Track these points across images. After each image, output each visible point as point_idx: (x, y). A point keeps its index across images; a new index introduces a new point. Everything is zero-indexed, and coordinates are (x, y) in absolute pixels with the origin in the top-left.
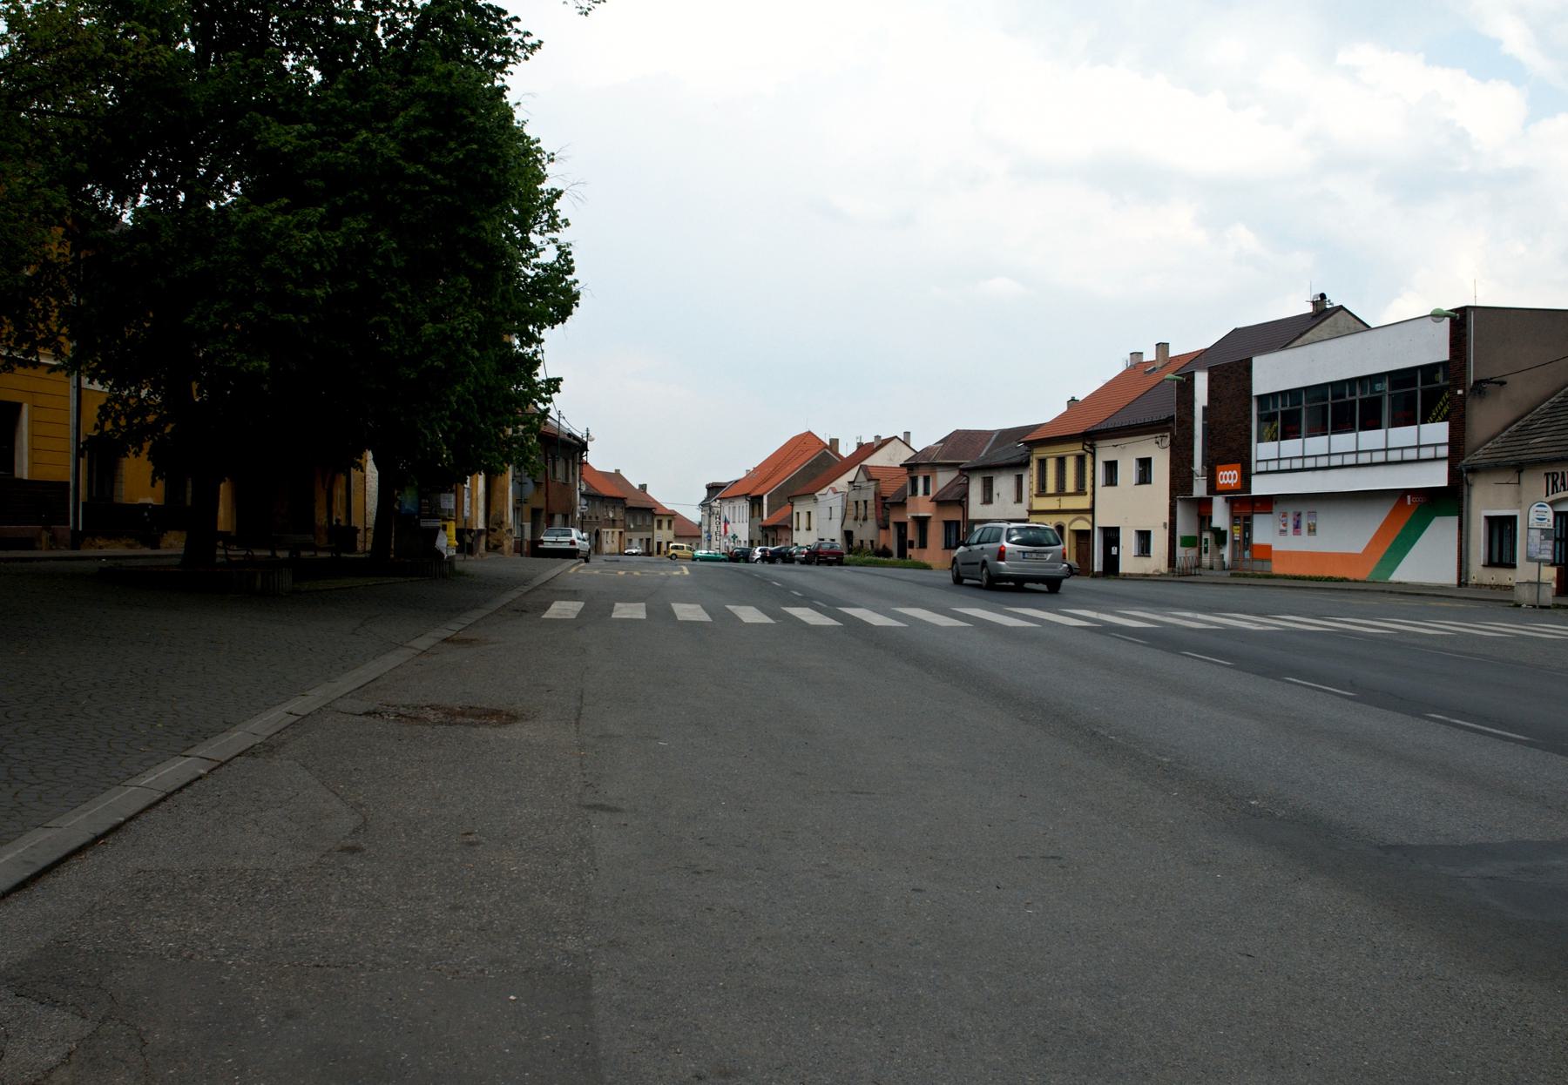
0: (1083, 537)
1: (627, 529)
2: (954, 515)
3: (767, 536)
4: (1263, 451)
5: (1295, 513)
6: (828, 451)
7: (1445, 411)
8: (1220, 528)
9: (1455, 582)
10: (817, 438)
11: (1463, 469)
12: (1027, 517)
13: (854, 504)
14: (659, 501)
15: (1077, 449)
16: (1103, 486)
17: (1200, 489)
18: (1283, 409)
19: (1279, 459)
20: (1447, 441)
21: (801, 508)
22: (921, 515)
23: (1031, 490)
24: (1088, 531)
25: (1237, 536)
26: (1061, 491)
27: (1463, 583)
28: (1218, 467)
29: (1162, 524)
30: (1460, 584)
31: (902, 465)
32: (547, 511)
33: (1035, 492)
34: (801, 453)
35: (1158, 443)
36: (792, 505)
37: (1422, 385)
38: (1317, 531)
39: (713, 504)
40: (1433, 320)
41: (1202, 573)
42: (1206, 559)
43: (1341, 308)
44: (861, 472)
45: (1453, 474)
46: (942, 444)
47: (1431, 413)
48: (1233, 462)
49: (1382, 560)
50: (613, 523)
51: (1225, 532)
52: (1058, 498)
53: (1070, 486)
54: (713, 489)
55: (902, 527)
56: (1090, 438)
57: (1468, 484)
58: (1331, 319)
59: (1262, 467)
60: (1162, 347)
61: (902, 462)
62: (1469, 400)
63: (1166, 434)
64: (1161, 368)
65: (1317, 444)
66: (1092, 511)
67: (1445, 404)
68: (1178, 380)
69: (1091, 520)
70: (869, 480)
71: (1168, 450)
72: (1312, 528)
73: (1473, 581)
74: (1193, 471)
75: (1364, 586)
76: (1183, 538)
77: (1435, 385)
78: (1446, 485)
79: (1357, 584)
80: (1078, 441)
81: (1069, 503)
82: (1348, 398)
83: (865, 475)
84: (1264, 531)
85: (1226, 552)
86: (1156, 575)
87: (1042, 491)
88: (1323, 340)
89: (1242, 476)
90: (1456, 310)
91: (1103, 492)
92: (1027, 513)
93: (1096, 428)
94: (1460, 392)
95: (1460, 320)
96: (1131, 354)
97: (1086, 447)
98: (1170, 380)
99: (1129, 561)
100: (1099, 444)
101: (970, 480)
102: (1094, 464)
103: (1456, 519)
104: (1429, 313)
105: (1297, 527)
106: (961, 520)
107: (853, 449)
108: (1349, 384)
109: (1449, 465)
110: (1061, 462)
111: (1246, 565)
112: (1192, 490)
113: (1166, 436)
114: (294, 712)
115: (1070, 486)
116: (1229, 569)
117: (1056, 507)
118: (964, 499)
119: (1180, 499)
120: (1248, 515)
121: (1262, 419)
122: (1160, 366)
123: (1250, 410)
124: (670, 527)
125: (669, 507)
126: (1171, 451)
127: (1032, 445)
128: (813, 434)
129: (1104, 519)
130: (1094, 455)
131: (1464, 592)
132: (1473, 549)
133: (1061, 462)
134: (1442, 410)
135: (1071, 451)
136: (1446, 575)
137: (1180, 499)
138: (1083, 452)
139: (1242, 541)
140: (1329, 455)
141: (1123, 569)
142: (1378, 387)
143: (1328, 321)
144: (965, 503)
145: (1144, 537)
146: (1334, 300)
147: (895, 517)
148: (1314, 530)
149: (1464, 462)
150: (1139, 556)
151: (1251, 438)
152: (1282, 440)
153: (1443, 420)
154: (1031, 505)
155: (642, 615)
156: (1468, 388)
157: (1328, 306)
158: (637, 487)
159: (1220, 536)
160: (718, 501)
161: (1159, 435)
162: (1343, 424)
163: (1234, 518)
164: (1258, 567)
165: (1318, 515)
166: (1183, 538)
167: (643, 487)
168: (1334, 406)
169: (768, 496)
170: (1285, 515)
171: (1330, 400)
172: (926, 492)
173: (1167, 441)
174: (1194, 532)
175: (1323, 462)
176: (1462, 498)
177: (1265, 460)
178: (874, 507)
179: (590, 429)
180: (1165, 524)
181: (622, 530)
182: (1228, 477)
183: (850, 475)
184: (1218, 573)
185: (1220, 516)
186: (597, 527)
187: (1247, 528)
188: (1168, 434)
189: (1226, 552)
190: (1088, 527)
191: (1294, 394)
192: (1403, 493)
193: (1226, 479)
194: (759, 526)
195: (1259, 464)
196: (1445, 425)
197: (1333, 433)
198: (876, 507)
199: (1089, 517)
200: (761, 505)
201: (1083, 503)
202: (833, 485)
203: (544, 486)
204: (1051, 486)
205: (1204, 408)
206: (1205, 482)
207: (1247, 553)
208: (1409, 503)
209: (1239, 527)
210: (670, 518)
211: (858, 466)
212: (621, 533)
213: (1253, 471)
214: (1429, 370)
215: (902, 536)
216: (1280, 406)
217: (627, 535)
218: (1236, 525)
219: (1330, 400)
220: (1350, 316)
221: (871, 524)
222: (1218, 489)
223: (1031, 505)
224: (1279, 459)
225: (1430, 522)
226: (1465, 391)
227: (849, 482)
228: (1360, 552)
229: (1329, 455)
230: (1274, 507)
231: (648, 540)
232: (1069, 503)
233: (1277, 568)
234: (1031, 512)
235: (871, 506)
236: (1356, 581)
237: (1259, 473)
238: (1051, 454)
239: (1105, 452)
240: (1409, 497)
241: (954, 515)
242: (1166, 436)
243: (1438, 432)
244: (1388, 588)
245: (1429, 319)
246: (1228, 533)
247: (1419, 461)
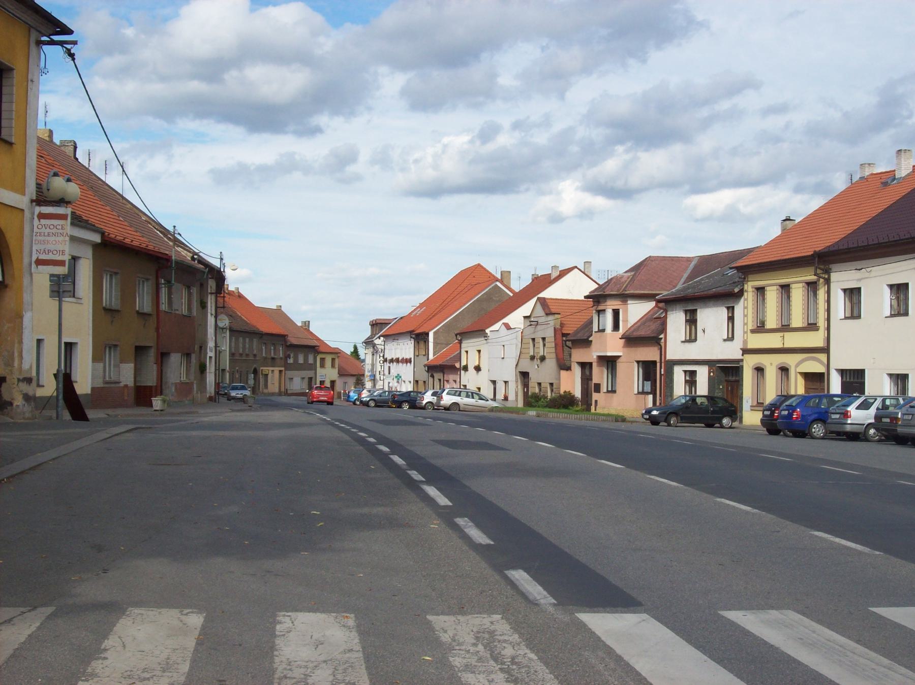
1: (288, 367)
2: (649, 354)
3: (433, 376)
6: (498, 284)
10: (488, 271)
12: (740, 357)
13: (531, 342)
14: (322, 338)
21: (470, 346)
22: (609, 354)
23: (745, 324)
24: (822, 375)
31: (585, 297)
32: (158, 349)
33: (750, 327)
34: (469, 287)
36: (460, 342)
39: (377, 342)
44: (539, 305)
46: (633, 273)
50: (273, 361)
52: (781, 334)
54: (377, 325)
55: (586, 366)
61: (587, 294)
66: (826, 350)
69: (826, 362)
70: (547, 314)
77: (726, 306)
83: (544, 309)
87: (760, 328)
91: (842, 329)
92: (741, 352)
93: (831, 249)
97: (819, 271)
100: (834, 267)
101: (668, 313)
106: (658, 360)
107: (527, 281)
118: (662, 336)
124: (333, 366)
125: (332, 345)
127: (748, 271)
128: (482, 267)
130: (828, 282)
135: (798, 281)
138: (815, 277)
144: (663, 341)
147: (579, 355)
154: (745, 342)
158: (299, 324)
160: (382, 338)
167: (307, 324)
169: (435, 333)
172: (616, 327)
178: (553, 345)
179: (223, 253)
181: (283, 369)
183: (527, 308)
186: (255, 366)
190: (820, 369)
194: (425, 366)
198: (556, 345)
199: (823, 357)
200: (426, 341)
201: (815, 339)
202: (505, 320)
203: (155, 317)
210: (333, 356)
211: (535, 299)
212: (280, 371)
215: (586, 379)
217: (290, 373)
221: (551, 363)
223: (745, 342)
227: (525, 317)
231: (310, 379)
232: (793, 340)
234: (746, 351)
235: (550, 343)
238: (772, 283)
241: (649, 354)
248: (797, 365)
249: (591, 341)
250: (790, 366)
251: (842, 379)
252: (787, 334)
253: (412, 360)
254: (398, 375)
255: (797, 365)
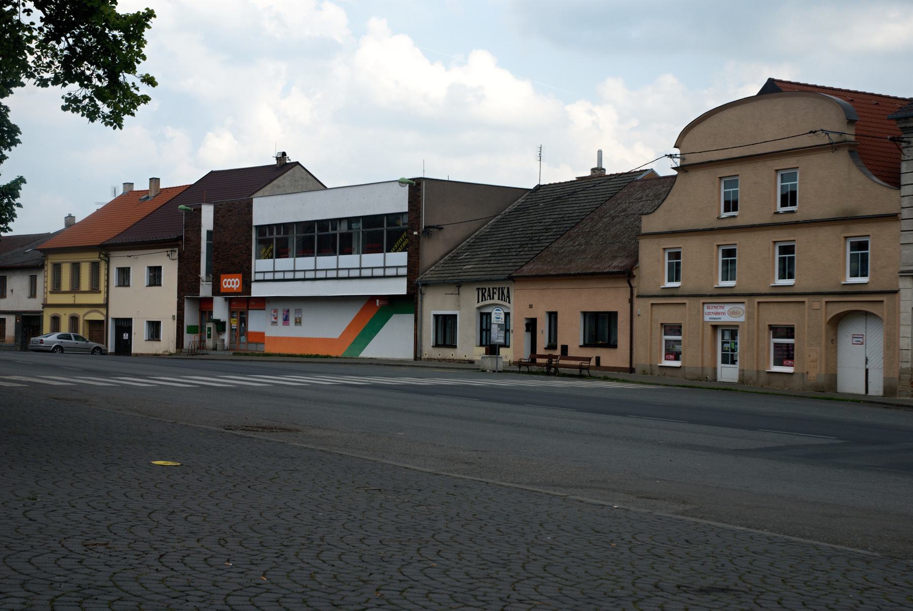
0: (97, 327)
4: (260, 265)
5: (284, 310)
7: (404, 244)
8: (220, 320)
9: (411, 356)
11: (420, 284)
15: (94, 257)
16: (116, 287)
17: (205, 290)
18: (279, 236)
19: (294, 271)
20: (406, 264)
24: (103, 321)
25: (234, 326)
26: (75, 288)
27: (419, 358)
28: (222, 276)
29: (171, 317)
30: (416, 358)
35: (168, 255)
37: (387, 226)
38: (303, 323)
40: (400, 185)
41: (208, 352)
42: (209, 343)
43: (297, 163)
45: (412, 287)
47: (394, 245)
48: (235, 273)
49: (353, 343)
51: (224, 323)
52: (73, 295)
53: (85, 284)
56: (106, 249)
57: (421, 293)
58: (291, 171)
59: (260, 277)
60: (155, 181)
62: (422, 238)
63: (175, 249)
64: (154, 197)
65: (305, 263)
66: (106, 305)
67: (403, 241)
68: (185, 210)
69: (105, 313)
71: (176, 262)
72: (298, 320)
73: (425, 356)
74: (200, 278)
75: (343, 361)
76: (188, 327)
78: (406, 294)
79: (338, 359)
80: (95, 251)
81: (81, 299)
82: (331, 232)
84: (257, 322)
85: (226, 337)
86: (165, 355)
88: (312, 191)
89: (243, 282)
90: (413, 179)
91: (117, 293)
93: (111, 242)
94: (415, 233)
95: (416, 187)
96: (124, 184)
97: (102, 256)
98: (182, 209)
99: (140, 343)
100: (113, 254)
102: (108, 269)
103: (412, 316)
104: (398, 179)
105: (286, 320)
108: (317, 222)
109: (407, 280)
110: (76, 267)
111: (243, 347)
112: (199, 292)
113: (175, 251)
114: (643, 382)
115: (85, 284)
116: (227, 350)
117: (71, 302)
119: (187, 298)
120: (244, 311)
121: (259, 242)
122: (153, 195)
123: (251, 236)
126: (179, 262)
129: (117, 310)
130: (108, 263)
131: (418, 363)
132: (425, 336)
133: (76, 267)
134: (402, 244)
136: (407, 353)
137: (187, 298)
139: (238, 330)
140: (315, 270)
141: (134, 350)
142: (354, 226)
143: (289, 173)
145: (154, 328)
146: (292, 158)
148: (300, 322)
149: (419, 279)
150: (149, 340)
151: (251, 255)
152: (276, 258)
153: (403, 251)
155: (537, 359)
156: (421, 231)
157: (288, 162)
159: (220, 326)
161: (170, 249)
162: (306, 250)
163: (231, 313)
164: (252, 348)
165: (303, 312)
166: (188, 327)
168: (319, 237)
170: (276, 311)
171: (316, 232)
173: (176, 255)
174: (196, 322)
175: (310, 275)
176: (417, 303)
177: (262, 272)
180: (174, 316)
182: (232, 283)
184: (221, 353)
185: (220, 311)
187: (243, 321)
188: (177, 249)
189: (226, 337)
190: (101, 318)
191: (287, 227)
192: (372, 299)
193: (229, 282)
195: (257, 274)
196: (405, 254)
197: (318, 255)
199: (104, 311)
201: (99, 299)
204: (66, 284)
205: (208, 232)
206: (211, 286)
207: (243, 339)
208: (378, 305)
209: (236, 319)
213: (253, 279)
214: (393, 218)
216: (275, 233)
218: (233, 317)
219: (316, 232)
220: (303, 170)
222: (222, 291)
224: (274, 272)
225: (390, 318)
226: (419, 233)
228: (337, 338)
229: (315, 270)
230: (266, 303)
232: (81, 299)
233: (268, 349)
236: (337, 357)
237: (257, 281)
239: (119, 261)
240: (378, 301)
242: (175, 251)
243: (399, 258)
244: (357, 361)
245: (397, 183)
246: (227, 323)
247: (385, 277)
248: (84, 316)
249: (73, 113)
250: (80, 316)
251: (116, 324)
252: (77, 295)
253: (447, 353)
254: (530, 305)
255: (84, 316)
